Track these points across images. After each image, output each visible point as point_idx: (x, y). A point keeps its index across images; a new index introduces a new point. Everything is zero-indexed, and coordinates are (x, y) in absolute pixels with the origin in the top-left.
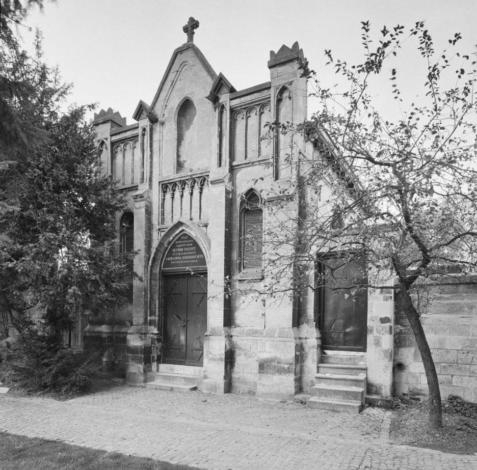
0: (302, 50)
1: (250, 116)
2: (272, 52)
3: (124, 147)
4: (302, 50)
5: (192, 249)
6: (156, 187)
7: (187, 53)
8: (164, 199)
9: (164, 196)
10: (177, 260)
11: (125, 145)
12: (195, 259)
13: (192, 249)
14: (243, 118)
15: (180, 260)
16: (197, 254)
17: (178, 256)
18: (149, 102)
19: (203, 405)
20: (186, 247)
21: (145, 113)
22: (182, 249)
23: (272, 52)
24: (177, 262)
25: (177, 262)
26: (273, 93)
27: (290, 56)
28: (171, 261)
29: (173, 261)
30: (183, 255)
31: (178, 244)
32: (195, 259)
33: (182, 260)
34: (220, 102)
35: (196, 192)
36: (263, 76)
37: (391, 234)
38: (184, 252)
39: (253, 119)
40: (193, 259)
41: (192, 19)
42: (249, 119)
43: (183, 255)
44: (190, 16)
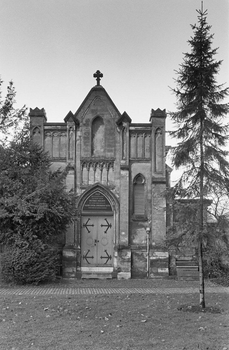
0: (125, 113)
1: (139, 137)
2: (153, 110)
3: (52, 134)
4: (125, 113)
5: (103, 201)
6: (78, 162)
7: (98, 94)
8: (82, 170)
9: (82, 168)
10: (93, 207)
11: (54, 133)
12: (105, 207)
13: (103, 201)
14: (135, 137)
15: (95, 207)
16: (106, 204)
17: (93, 204)
18: (74, 113)
19: (99, 244)
20: (99, 200)
21: (71, 119)
22: (97, 205)
23: (153, 110)
24: (93, 208)
25: (93, 208)
26: (154, 129)
27: (159, 114)
28: (88, 207)
29: (89, 207)
30: (97, 204)
31: (92, 197)
32: (105, 207)
33: (96, 207)
34: (123, 126)
35: (105, 170)
36: (146, 120)
37: (179, 185)
38: (97, 200)
39: (140, 138)
40: (104, 207)
41: (98, 72)
42: (138, 138)
43: (97, 204)
44: (98, 70)
